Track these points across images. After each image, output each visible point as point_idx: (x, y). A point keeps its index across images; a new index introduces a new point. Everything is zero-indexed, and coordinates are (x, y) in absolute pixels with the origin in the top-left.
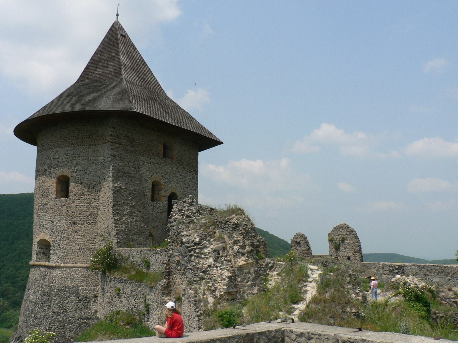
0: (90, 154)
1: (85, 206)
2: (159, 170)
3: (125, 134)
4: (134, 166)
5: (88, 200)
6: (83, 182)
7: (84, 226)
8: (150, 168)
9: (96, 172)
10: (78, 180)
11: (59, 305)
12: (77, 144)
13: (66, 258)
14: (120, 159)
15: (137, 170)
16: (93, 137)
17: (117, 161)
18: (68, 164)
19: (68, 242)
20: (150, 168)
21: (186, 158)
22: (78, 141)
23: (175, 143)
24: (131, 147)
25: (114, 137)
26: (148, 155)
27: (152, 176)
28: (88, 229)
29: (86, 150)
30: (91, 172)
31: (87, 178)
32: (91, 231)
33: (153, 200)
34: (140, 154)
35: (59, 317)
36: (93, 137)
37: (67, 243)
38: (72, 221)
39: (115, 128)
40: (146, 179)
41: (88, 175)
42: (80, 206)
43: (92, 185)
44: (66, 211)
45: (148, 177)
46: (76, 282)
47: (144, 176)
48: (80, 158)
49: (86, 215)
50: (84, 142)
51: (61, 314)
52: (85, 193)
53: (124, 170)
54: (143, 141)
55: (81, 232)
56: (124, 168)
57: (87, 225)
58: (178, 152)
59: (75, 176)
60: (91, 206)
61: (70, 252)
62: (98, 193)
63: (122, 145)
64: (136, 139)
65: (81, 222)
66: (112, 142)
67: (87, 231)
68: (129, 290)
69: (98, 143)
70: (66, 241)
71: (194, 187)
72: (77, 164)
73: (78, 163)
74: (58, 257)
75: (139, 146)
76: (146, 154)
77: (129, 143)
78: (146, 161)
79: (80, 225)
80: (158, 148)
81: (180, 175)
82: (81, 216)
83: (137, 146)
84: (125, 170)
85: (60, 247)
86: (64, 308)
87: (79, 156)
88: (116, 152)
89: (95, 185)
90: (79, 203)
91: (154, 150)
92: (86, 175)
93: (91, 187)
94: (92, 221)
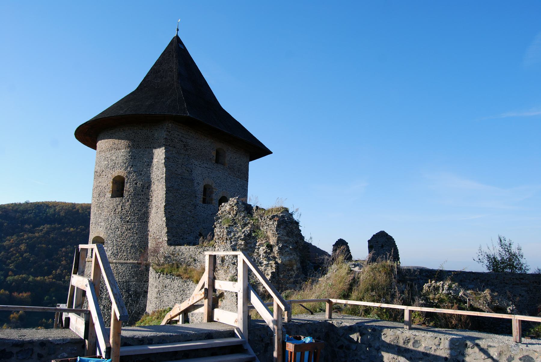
5: (142, 199)
8: (202, 172)
14: (173, 161)
16: (148, 140)
20: (202, 172)
25: (168, 140)
27: (204, 179)
32: (143, 229)
33: (204, 201)
36: (148, 140)
45: (200, 180)
48: (136, 160)
50: (140, 145)
54: (197, 147)
63: (176, 148)
68: (176, 286)
69: (153, 146)
83: (191, 151)
93: (145, 188)
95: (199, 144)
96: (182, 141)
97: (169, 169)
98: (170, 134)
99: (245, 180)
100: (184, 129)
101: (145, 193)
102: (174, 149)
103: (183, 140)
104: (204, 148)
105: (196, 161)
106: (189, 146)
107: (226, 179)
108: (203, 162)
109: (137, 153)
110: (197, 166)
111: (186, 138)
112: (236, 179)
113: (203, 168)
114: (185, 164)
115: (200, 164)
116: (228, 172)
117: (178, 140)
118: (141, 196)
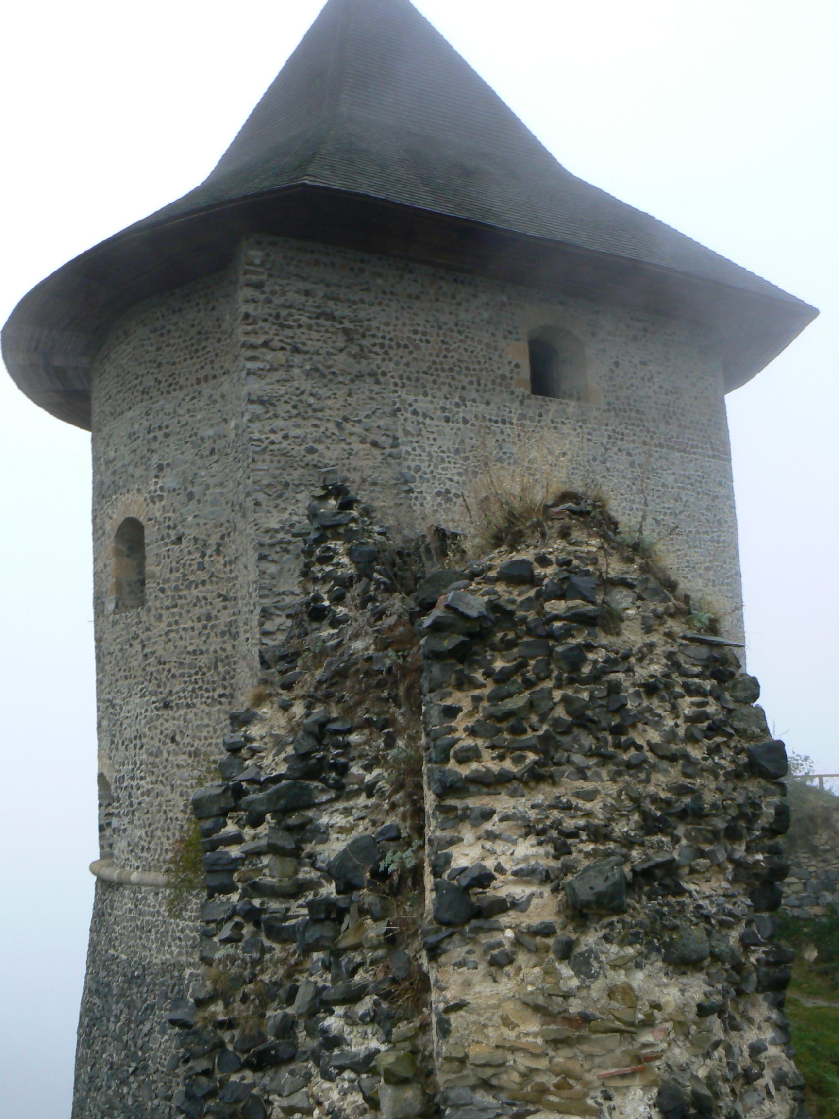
0: (199, 416)
1: (193, 629)
2: (514, 450)
3: (318, 307)
4: (371, 437)
5: (203, 603)
6: (183, 534)
7: (196, 715)
8: (462, 442)
9: (221, 484)
10: (169, 527)
11: (125, 1038)
12: (159, 390)
13: (149, 849)
14: (294, 412)
15: (388, 451)
16: (204, 348)
17: (280, 423)
18: (138, 472)
19: (152, 783)
20: (462, 442)
21: (655, 392)
22: (160, 377)
23: (594, 334)
24: (354, 356)
25: (261, 324)
26: (445, 388)
28: (207, 726)
29: (186, 406)
30: (208, 487)
31: (195, 516)
32: (219, 732)
34: (403, 385)
35: (125, 1090)
36: (204, 348)
37: (150, 786)
38: (160, 696)
39: (259, 286)
40: (448, 492)
41: (199, 501)
42: (177, 631)
43: (213, 541)
44: (140, 657)
45: (456, 478)
46: (173, 948)
47: (434, 477)
48: (172, 440)
49: (200, 668)
51: (131, 1079)
52: (192, 578)
53: (315, 456)
55: (187, 740)
56: (320, 447)
57: (204, 707)
58: (612, 371)
59: (158, 515)
60: (213, 627)
61: (159, 821)
62: (231, 571)
63: (307, 352)
64: (375, 324)
65: (185, 698)
66: (253, 347)
67: (205, 734)
70: (148, 779)
71: (708, 509)
72: (160, 468)
73: (165, 463)
74: (129, 845)
75: (392, 353)
76: (434, 382)
77: (341, 344)
78: (439, 413)
79: (182, 712)
80: (500, 356)
81: (632, 464)
82: (182, 675)
83: (386, 353)
84: (322, 455)
85: (131, 805)
86: (140, 1054)
87: (167, 435)
88: (276, 386)
89: (223, 537)
90: (176, 622)
91: (477, 367)
92: (193, 505)
93: (209, 552)
94: (220, 691)
95: (430, 318)
96: (331, 317)
97: (271, 447)
98: (263, 293)
99: (711, 453)
100: (333, 264)
101: (212, 576)
102: (297, 359)
103: (336, 313)
104: (460, 332)
105: (421, 397)
106: (374, 336)
107: (599, 459)
108: (463, 399)
109: (172, 411)
110: (432, 419)
111: (355, 303)
112: (657, 455)
113: (465, 421)
114: (357, 415)
115: (444, 409)
116: (610, 428)
117: (310, 318)
118: (200, 587)
